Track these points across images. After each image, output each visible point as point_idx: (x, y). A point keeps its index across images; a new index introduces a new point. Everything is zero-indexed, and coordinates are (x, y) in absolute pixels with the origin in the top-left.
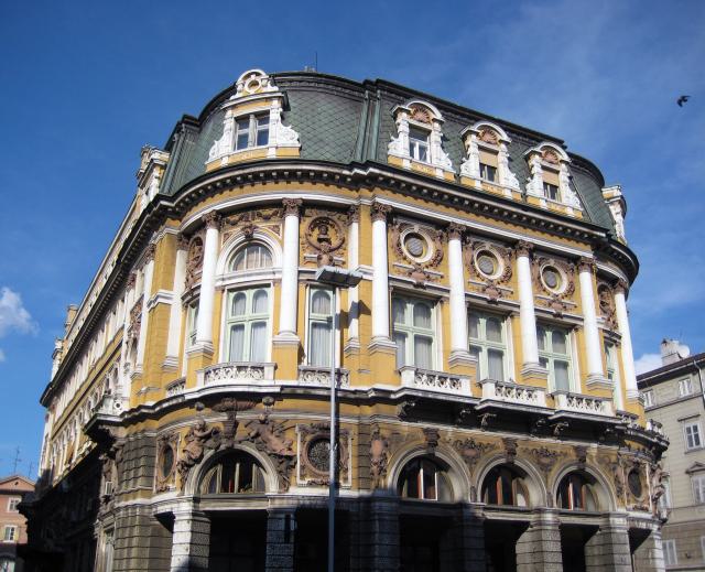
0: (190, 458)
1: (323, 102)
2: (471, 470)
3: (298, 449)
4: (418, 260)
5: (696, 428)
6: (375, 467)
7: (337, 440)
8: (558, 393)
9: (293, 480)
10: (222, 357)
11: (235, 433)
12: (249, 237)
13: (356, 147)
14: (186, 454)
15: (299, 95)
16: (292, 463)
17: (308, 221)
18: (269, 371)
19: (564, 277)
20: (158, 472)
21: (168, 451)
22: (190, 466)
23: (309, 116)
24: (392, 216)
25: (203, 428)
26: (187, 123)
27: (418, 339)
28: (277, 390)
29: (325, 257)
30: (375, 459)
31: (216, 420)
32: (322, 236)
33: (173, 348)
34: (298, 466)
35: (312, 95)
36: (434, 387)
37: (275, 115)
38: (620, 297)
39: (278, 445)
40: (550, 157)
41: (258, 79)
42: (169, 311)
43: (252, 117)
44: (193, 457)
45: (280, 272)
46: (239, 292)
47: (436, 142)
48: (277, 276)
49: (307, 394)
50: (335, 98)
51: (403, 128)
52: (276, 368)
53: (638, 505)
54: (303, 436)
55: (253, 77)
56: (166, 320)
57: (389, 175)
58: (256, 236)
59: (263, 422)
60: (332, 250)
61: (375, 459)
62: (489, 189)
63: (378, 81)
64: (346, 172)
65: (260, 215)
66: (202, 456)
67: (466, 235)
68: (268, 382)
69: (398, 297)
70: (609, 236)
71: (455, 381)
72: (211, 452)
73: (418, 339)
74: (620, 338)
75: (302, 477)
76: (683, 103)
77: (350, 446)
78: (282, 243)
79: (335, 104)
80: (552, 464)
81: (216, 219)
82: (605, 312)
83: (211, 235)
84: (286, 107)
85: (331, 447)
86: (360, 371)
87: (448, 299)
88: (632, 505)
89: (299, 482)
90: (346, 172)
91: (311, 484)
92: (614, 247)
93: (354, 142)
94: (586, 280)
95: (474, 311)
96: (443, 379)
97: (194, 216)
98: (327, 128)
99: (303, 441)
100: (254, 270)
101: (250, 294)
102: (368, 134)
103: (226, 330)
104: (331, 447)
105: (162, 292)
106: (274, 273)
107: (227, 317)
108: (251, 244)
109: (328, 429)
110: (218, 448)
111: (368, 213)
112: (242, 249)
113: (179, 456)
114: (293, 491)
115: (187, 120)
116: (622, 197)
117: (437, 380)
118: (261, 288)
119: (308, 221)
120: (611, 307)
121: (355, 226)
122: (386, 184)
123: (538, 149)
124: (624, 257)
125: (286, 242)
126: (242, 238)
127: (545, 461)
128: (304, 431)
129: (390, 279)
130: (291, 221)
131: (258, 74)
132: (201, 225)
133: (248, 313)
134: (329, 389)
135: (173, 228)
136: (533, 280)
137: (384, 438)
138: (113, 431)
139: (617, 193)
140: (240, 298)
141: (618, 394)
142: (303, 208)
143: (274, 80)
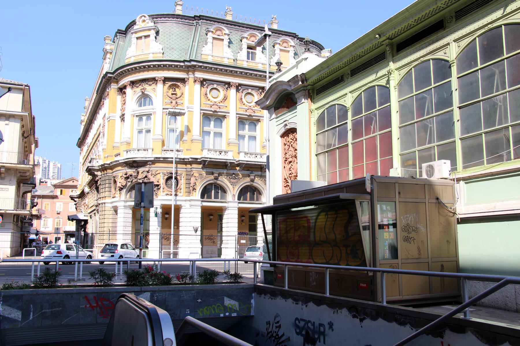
1: (175, 28)
2: (233, 188)
3: (162, 182)
4: (215, 100)
5: (171, 195)
9: (159, 193)
10: (134, 146)
20: (113, 189)
21: (115, 182)
22: (122, 189)
23: (165, 41)
24: (203, 82)
25: (126, 174)
26: (120, 33)
27: (215, 133)
28: (153, 159)
29: (174, 102)
30: (191, 185)
31: (131, 171)
33: (117, 139)
41: (145, 19)
42: (115, 122)
43: (143, 37)
46: (140, 117)
49: (165, 160)
50: (181, 25)
51: (210, 40)
52: (153, 150)
57: (201, 64)
58: (146, 93)
59: (148, 172)
60: (177, 98)
63: (200, 16)
66: (126, 185)
68: (149, 155)
69: (206, 117)
72: (129, 183)
73: (215, 133)
75: (163, 192)
78: (156, 96)
83: (129, 90)
84: (157, 33)
85: (173, 181)
86: (187, 150)
96: (220, 152)
97: (123, 82)
101: (144, 118)
105: (111, 114)
107: (136, 127)
108: (144, 97)
110: (132, 181)
112: (141, 98)
113: (119, 185)
115: (120, 32)
118: (149, 116)
121: (187, 87)
123: (278, 42)
126: (141, 93)
127: (410, 162)
129: (201, 110)
130: (160, 85)
132: (125, 87)
134: (172, 158)
135: (113, 88)
138: (96, 173)
142: (166, 80)
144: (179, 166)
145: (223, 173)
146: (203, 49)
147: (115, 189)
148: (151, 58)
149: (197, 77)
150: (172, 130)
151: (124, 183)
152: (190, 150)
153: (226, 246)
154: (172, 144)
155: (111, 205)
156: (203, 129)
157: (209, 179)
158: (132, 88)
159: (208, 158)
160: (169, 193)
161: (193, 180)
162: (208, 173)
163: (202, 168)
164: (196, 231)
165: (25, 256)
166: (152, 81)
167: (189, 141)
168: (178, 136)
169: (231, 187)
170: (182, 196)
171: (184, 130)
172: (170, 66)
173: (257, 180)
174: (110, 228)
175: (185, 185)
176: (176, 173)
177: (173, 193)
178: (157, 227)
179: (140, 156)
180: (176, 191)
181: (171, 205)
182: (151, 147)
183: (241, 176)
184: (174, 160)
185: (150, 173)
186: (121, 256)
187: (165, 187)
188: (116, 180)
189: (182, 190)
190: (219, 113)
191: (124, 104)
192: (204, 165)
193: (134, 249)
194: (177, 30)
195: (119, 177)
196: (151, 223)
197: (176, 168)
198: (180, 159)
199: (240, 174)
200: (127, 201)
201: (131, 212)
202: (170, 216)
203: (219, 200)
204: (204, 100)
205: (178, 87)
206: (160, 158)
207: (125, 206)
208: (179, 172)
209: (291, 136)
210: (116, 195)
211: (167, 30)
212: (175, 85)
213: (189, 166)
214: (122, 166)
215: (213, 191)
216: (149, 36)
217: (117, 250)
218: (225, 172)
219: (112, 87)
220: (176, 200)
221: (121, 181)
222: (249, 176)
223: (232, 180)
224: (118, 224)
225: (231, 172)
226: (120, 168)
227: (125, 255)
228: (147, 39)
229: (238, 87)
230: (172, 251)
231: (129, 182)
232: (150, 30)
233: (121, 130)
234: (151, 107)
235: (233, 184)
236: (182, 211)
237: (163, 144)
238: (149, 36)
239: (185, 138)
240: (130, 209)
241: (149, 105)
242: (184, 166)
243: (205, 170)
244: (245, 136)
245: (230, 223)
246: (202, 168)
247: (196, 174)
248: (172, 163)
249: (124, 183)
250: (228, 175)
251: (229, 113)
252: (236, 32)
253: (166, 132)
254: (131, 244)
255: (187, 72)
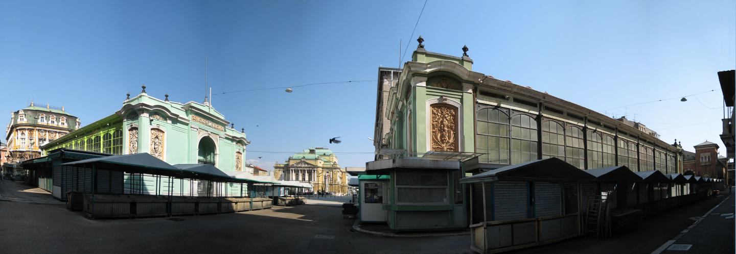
10: (21, 147)
24: (38, 130)
49: (29, 151)
51: (40, 118)
68: (24, 150)
76: (423, 44)
83: (19, 131)
92: (255, 184)
100: (23, 137)
122: (38, 126)
135: (15, 129)
142: (28, 129)
196: (384, 120)
209: (134, 131)
229: (49, 131)
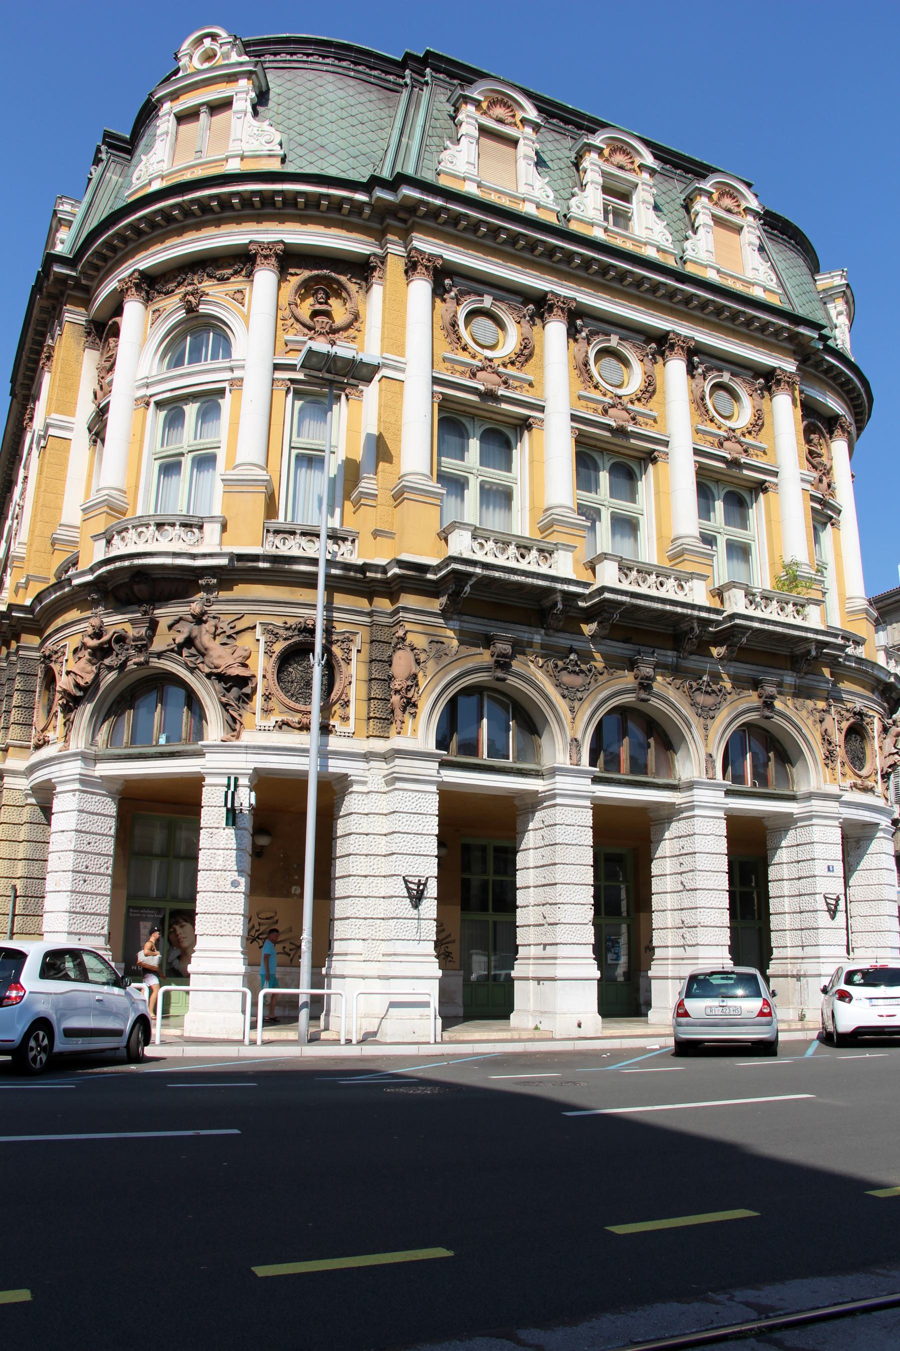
0: (77, 686)
1: (330, 87)
2: (572, 710)
3: (261, 666)
6: (396, 699)
7: (327, 649)
8: (732, 585)
9: (246, 717)
11: (151, 639)
12: (191, 309)
13: (383, 160)
14: (71, 677)
15: (287, 74)
16: (247, 690)
17: (294, 281)
18: (212, 530)
19: (746, 401)
21: (50, 679)
24: (444, 278)
25: (98, 634)
28: (224, 561)
31: (117, 622)
32: (318, 307)
34: (260, 691)
35: (310, 75)
36: (508, 559)
37: (243, 104)
38: (839, 448)
39: (222, 657)
40: (727, 202)
42: (67, 450)
43: (203, 109)
44: (82, 683)
45: (242, 367)
46: (172, 407)
47: (526, 157)
48: (237, 374)
49: (281, 571)
50: (352, 82)
51: (469, 129)
52: (224, 528)
53: (859, 782)
54: (269, 644)
55: (207, 42)
56: (62, 465)
57: (439, 202)
59: (199, 619)
60: (334, 331)
61: (396, 685)
62: (618, 243)
64: (361, 197)
65: (210, 276)
67: (577, 318)
68: (210, 546)
69: (452, 421)
70: (824, 338)
71: (546, 553)
72: (111, 676)
74: (839, 512)
75: (267, 711)
77: (354, 663)
78: (246, 318)
79: (351, 91)
80: (717, 707)
81: (138, 287)
82: (814, 467)
83: (133, 309)
85: (316, 662)
86: (376, 534)
87: (542, 421)
88: (848, 782)
89: (259, 720)
90: (361, 197)
91: (283, 725)
93: (381, 153)
94: (784, 410)
95: (588, 454)
96: (524, 548)
98: (334, 127)
99: (268, 653)
101: (191, 410)
102: (404, 140)
103: (150, 469)
104: (316, 662)
106: (231, 369)
109: (312, 632)
110: (123, 665)
111: (402, 268)
112: (181, 337)
113: (64, 682)
114: (248, 737)
116: (848, 285)
117: (512, 550)
118: (209, 399)
119: (294, 281)
120: (824, 459)
121: (377, 290)
124: (849, 380)
125: (257, 314)
126: (181, 314)
128: (272, 633)
130: (265, 277)
131: (214, 37)
133: (188, 436)
134: (314, 562)
135: (74, 317)
136: (693, 401)
137: (413, 649)
139: (838, 281)
140: (175, 420)
141: (832, 600)
142: (289, 259)
143: (247, 47)
144: (341, 600)
145: (530, 644)
146: (445, 155)
147: (51, 702)
148: (234, 166)
149: (421, 253)
150: (310, 460)
151: (85, 671)
152: (389, 535)
153: (791, 969)
154: (308, 500)
155: (24, 784)
156: (439, 464)
157: (470, 664)
158: (148, 300)
159: (474, 563)
160: (295, 718)
161: (402, 663)
162: (467, 639)
163: (445, 614)
164: (416, 898)
165: (298, 987)
166: (230, 266)
167: (385, 497)
168: (333, 482)
169: (562, 705)
170: (350, 737)
171: (359, 458)
172: (313, 201)
173: (660, 683)
174: (19, 884)
175: (364, 687)
176: (328, 631)
177: (315, 720)
178: (235, 876)
179: (165, 547)
180: (326, 709)
181: (306, 773)
182: (217, 511)
183: (599, 664)
184: (321, 570)
185: (209, 626)
186: (42, 1024)
187: (276, 689)
188: (56, 667)
189: (352, 711)
190: (504, 406)
191: (111, 369)
192: (454, 597)
193: (118, 982)
194: (341, 94)
195: (69, 652)
197: (329, 607)
198: (347, 567)
199: (598, 656)
200: (97, 759)
201: (111, 808)
202: (289, 835)
203: (509, 762)
204: (445, 350)
205: (338, 291)
206: (256, 558)
207: (85, 781)
208: (339, 628)
210: (50, 735)
211: (300, 90)
212: (329, 281)
213: (383, 604)
214: (84, 605)
215: (485, 721)
216: (226, 104)
217: (15, 983)
218: (537, 639)
219: (67, 316)
220: (324, 754)
221: (73, 670)
222: (632, 665)
223: (566, 678)
224: (53, 862)
225: (563, 641)
226: (74, 614)
227: (62, 1017)
228: (220, 118)
230: (304, 991)
231: (110, 668)
232: (232, 78)
233: (90, 476)
234: (221, 363)
235: (569, 694)
236: (351, 803)
237: (271, 509)
238: (226, 104)
239: (367, 484)
240: (111, 794)
241: (215, 357)
242: (362, 603)
243: (456, 624)
244: (598, 512)
245: (556, 876)
246: (445, 614)
247: (419, 641)
248: (314, 586)
249: (85, 671)
250: (548, 652)
251: (542, 409)
252: (558, 137)
253: (285, 462)
254: (108, 956)
255: (380, 236)
